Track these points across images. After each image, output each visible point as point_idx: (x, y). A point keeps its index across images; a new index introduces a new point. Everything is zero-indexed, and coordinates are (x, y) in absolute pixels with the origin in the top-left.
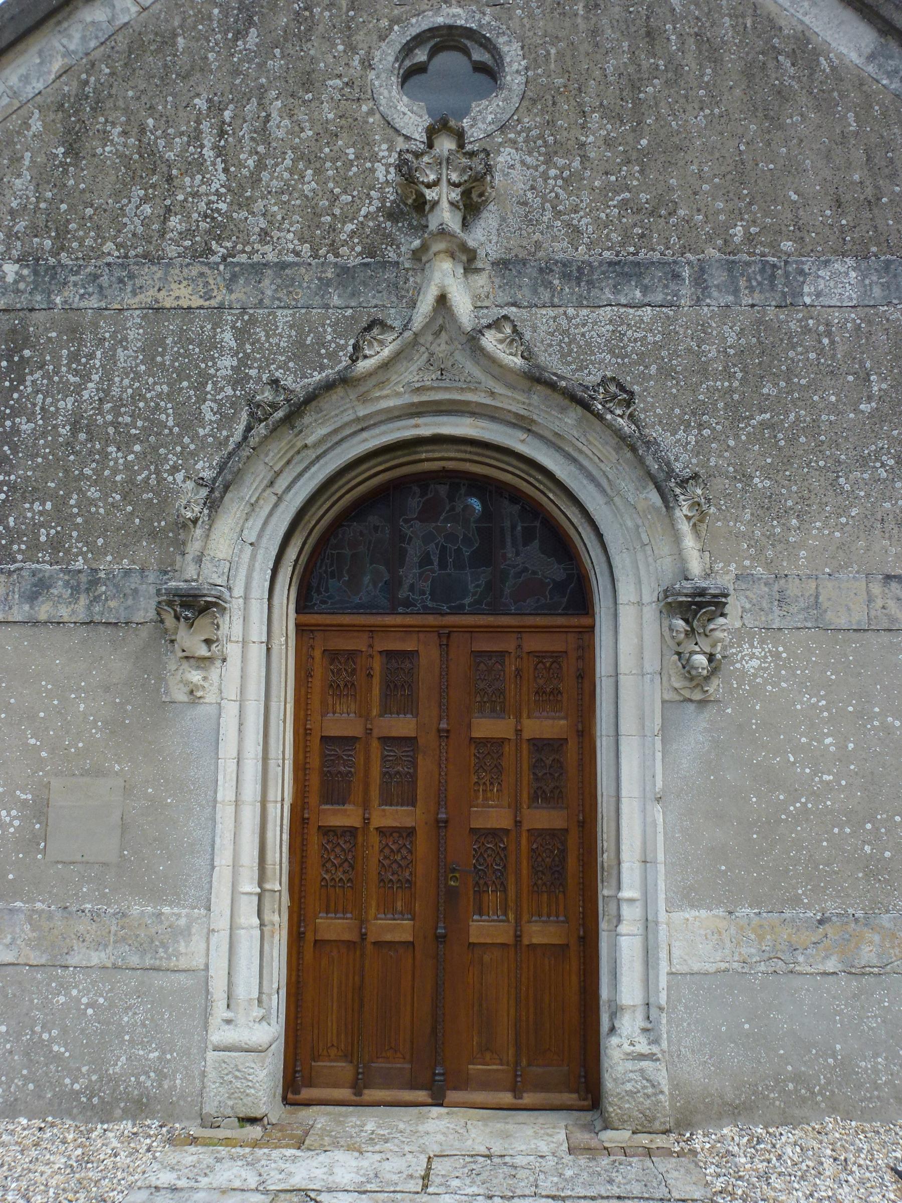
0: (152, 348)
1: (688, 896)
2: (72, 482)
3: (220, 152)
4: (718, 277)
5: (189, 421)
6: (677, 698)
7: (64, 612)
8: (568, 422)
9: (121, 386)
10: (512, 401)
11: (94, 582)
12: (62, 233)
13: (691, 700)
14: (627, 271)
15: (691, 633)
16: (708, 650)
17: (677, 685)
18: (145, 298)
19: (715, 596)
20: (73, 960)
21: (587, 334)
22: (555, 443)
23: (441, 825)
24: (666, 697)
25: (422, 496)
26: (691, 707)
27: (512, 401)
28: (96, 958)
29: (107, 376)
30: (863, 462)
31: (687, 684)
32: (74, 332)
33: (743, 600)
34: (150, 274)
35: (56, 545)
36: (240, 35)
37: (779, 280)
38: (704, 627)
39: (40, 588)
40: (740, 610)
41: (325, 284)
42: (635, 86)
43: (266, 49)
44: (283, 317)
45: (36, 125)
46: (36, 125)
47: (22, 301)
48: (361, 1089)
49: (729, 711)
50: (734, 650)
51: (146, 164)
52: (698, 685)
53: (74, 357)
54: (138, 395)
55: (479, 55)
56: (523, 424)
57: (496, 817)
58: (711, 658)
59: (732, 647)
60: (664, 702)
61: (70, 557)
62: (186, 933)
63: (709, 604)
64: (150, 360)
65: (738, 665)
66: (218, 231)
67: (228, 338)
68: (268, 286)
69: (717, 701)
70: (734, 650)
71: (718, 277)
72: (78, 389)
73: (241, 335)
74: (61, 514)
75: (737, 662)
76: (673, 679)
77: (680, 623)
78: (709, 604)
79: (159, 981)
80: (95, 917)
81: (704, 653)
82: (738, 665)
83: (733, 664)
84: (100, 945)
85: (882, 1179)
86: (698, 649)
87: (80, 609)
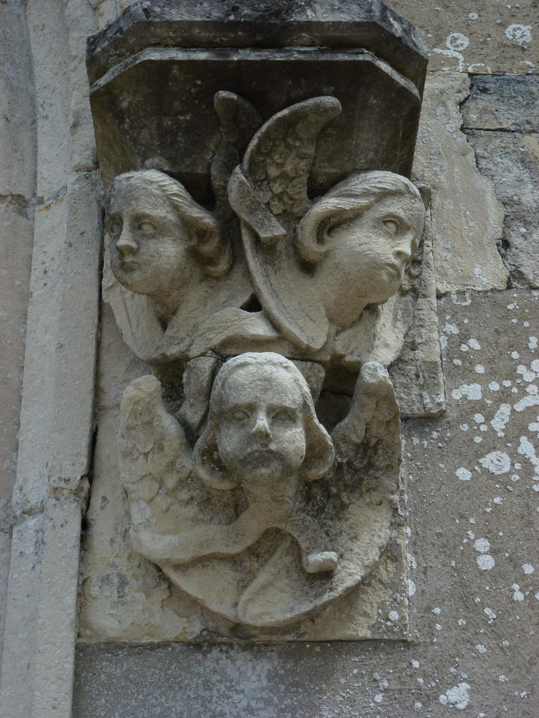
6: (174, 626)
13: (241, 638)
15: (219, 248)
16: (314, 334)
17: (158, 544)
19: (334, 38)
24: (110, 621)
26: (251, 676)
31: (215, 537)
33: (510, 172)
38: (291, 218)
40: (495, 215)
49: (458, 695)
50: (474, 391)
52: (272, 537)
58: (338, 387)
59: (466, 374)
60: (87, 653)
63: (309, 77)
65: (497, 462)
69: (392, 644)
70: (474, 391)
75: (492, 443)
76: (139, 513)
77: (154, 186)
78: (309, 77)
81: (300, 354)
82: (497, 462)
83: (473, 456)
85: (395, 699)
86: (257, 327)
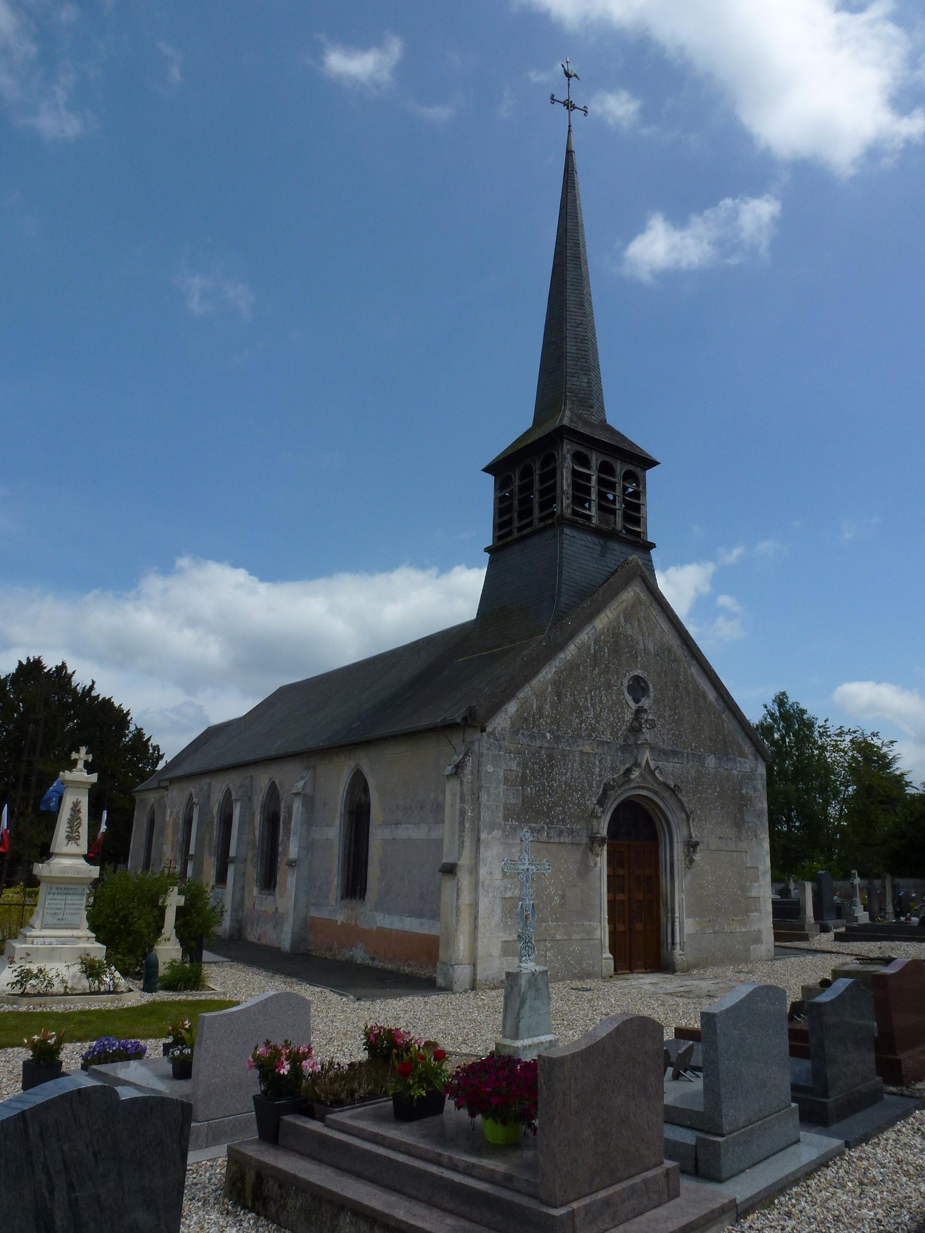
0: (582, 763)
1: (688, 917)
2: (566, 802)
3: (592, 705)
4: (691, 758)
5: (591, 787)
7: (567, 840)
8: (667, 795)
9: (575, 773)
10: (656, 787)
11: (573, 832)
12: (558, 726)
14: (675, 753)
18: (579, 748)
20: (574, 938)
21: (670, 770)
22: (662, 798)
23: (630, 899)
25: (747, 758)
27: (656, 787)
28: (578, 937)
29: (572, 771)
30: (715, 808)
32: (563, 756)
34: (580, 741)
35: (563, 820)
36: (594, 669)
37: (701, 759)
39: (560, 833)
41: (617, 749)
42: (674, 701)
43: (600, 673)
44: (609, 758)
45: (550, 689)
46: (550, 689)
47: (552, 746)
48: (631, 969)
51: (575, 706)
53: (564, 764)
54: (579, 778)
55: (643, 685)
56: (655, 793)
57: (641, 897)
61: (567, 824)
62: (595, 929)
64: (581, 767)
66: (594, 730)
67: (597, 762)
68: (605, 748)
71: (691, 758)
72: (566, 774)
73: (600, 762)
74: (565, 813)
79: (592, 942)
80: (578, 926)
84: (579, 934)
87: (568, 840)
